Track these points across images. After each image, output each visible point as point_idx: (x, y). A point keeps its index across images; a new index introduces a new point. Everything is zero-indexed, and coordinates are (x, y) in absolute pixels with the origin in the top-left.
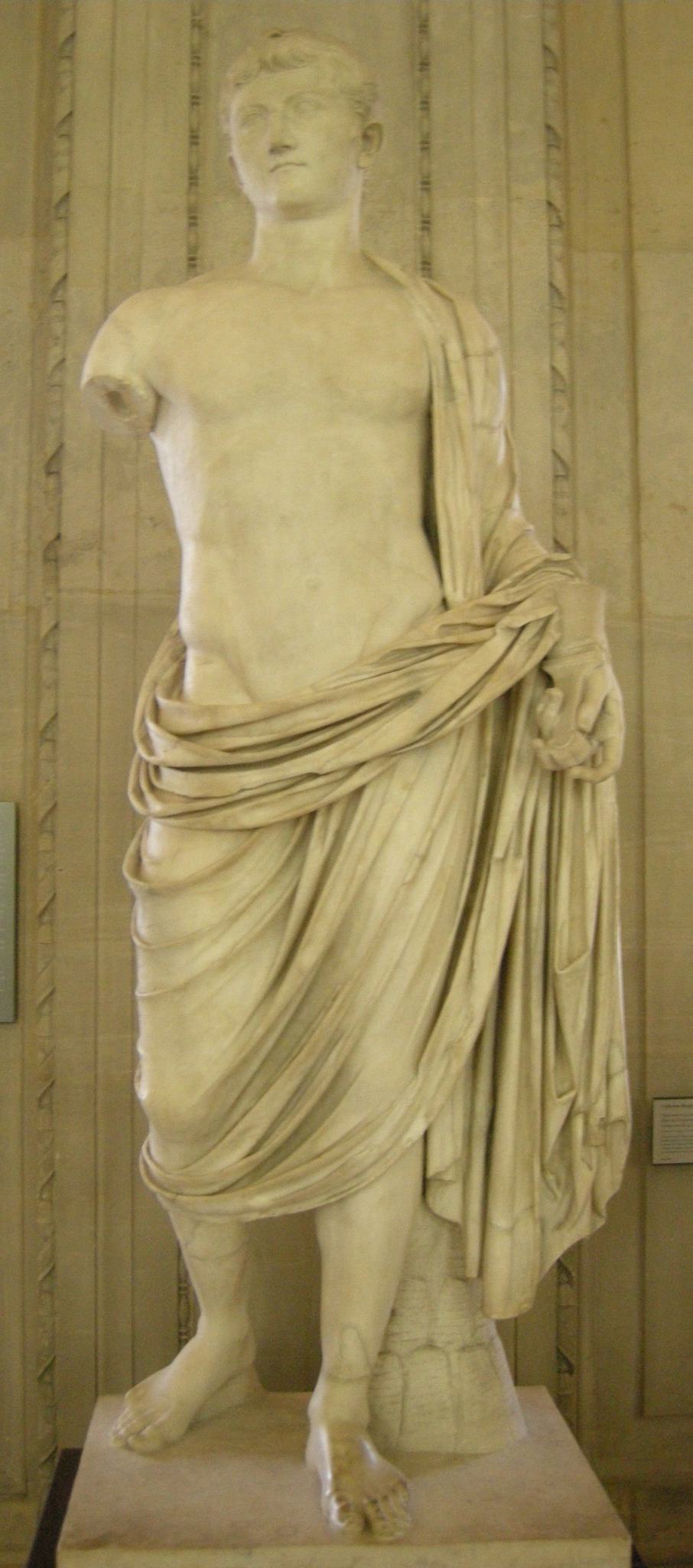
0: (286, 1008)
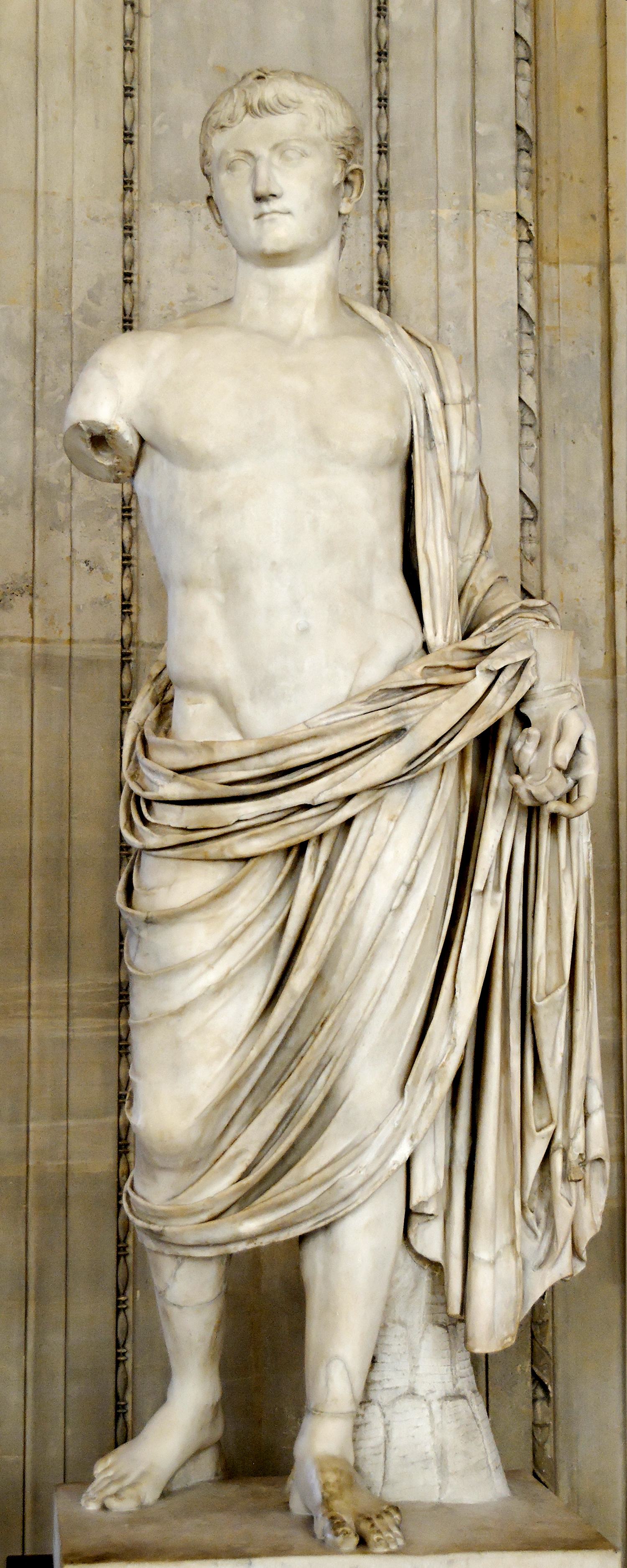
0: (277, 1032)
